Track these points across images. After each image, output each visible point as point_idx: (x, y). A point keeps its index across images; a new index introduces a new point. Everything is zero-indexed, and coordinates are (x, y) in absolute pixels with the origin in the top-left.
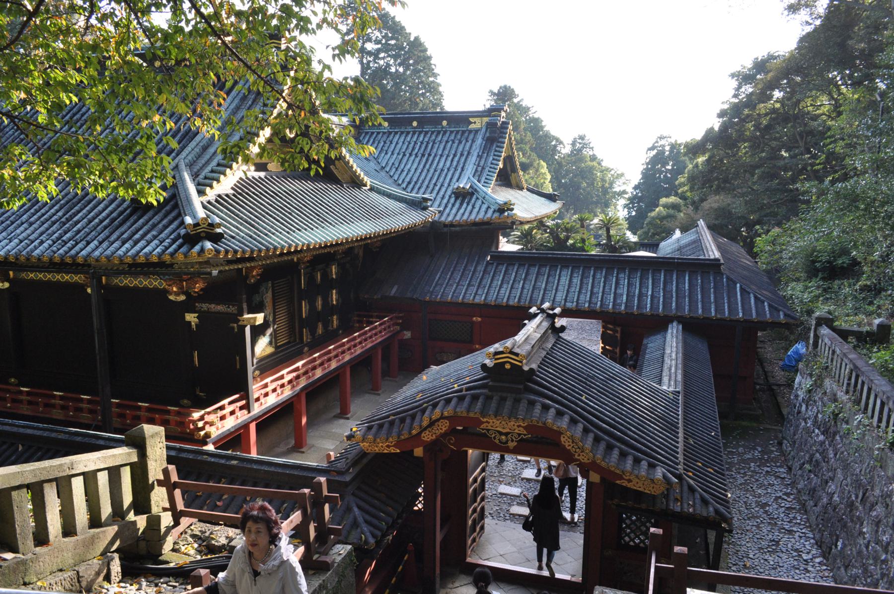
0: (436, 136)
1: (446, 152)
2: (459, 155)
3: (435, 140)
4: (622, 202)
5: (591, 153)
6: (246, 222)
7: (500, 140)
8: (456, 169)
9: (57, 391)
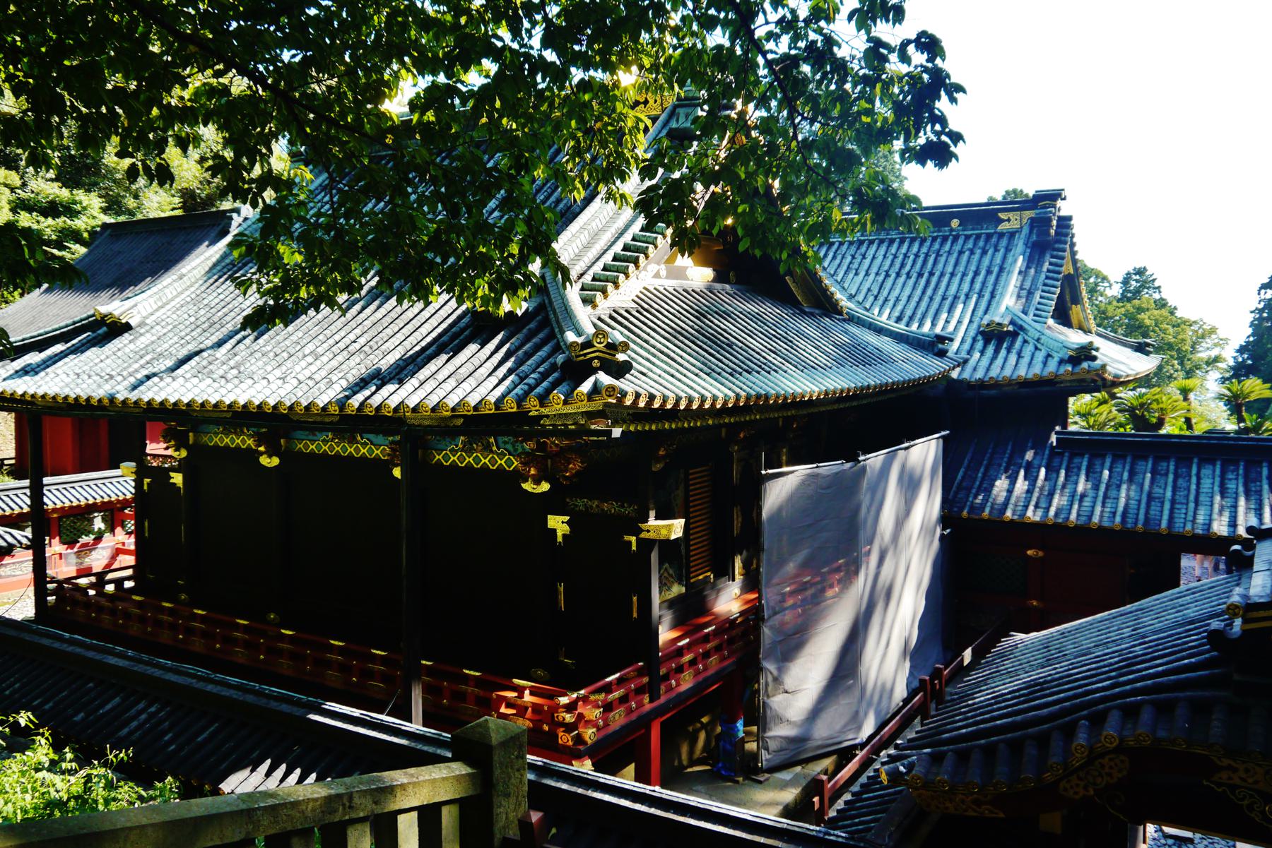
0: (942, 245)
1: (961, 268)
2: (983, 273)
3: (939, 251)
4: (1214, 375)
5: (1157, 296)
6: (662, 352)
7: (1057, 246)
8: (980, 296)
9: (199, 609)
